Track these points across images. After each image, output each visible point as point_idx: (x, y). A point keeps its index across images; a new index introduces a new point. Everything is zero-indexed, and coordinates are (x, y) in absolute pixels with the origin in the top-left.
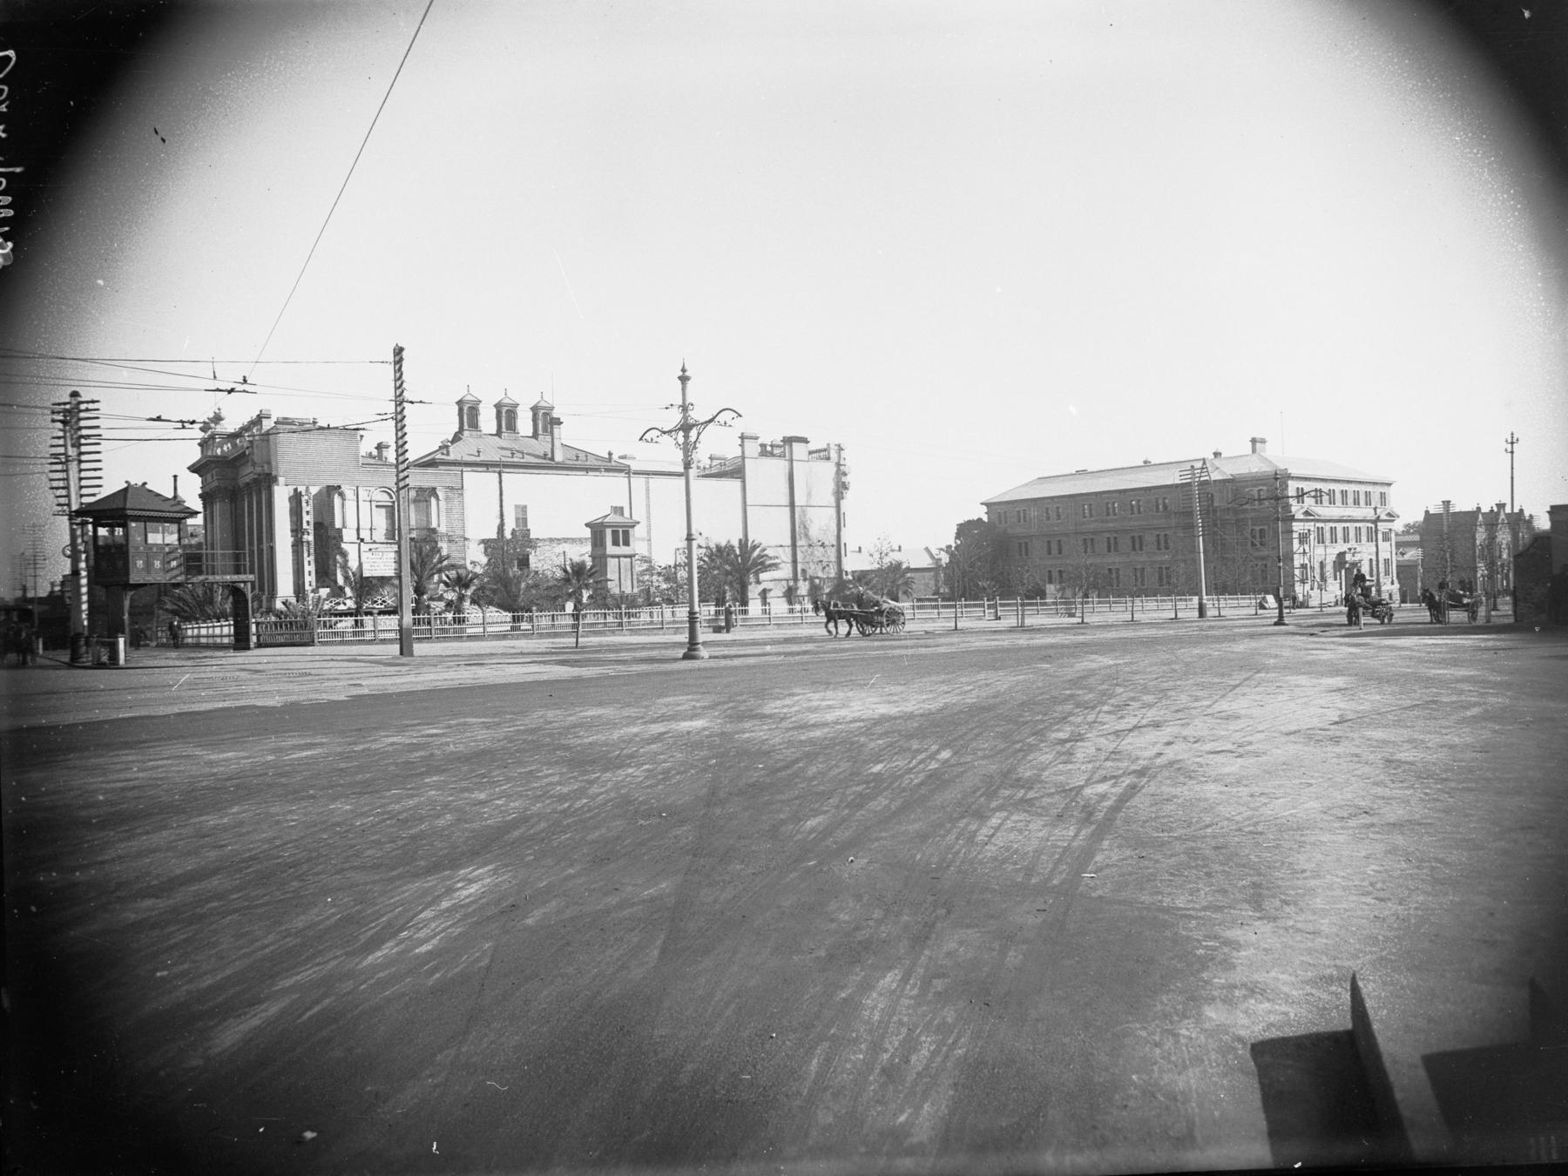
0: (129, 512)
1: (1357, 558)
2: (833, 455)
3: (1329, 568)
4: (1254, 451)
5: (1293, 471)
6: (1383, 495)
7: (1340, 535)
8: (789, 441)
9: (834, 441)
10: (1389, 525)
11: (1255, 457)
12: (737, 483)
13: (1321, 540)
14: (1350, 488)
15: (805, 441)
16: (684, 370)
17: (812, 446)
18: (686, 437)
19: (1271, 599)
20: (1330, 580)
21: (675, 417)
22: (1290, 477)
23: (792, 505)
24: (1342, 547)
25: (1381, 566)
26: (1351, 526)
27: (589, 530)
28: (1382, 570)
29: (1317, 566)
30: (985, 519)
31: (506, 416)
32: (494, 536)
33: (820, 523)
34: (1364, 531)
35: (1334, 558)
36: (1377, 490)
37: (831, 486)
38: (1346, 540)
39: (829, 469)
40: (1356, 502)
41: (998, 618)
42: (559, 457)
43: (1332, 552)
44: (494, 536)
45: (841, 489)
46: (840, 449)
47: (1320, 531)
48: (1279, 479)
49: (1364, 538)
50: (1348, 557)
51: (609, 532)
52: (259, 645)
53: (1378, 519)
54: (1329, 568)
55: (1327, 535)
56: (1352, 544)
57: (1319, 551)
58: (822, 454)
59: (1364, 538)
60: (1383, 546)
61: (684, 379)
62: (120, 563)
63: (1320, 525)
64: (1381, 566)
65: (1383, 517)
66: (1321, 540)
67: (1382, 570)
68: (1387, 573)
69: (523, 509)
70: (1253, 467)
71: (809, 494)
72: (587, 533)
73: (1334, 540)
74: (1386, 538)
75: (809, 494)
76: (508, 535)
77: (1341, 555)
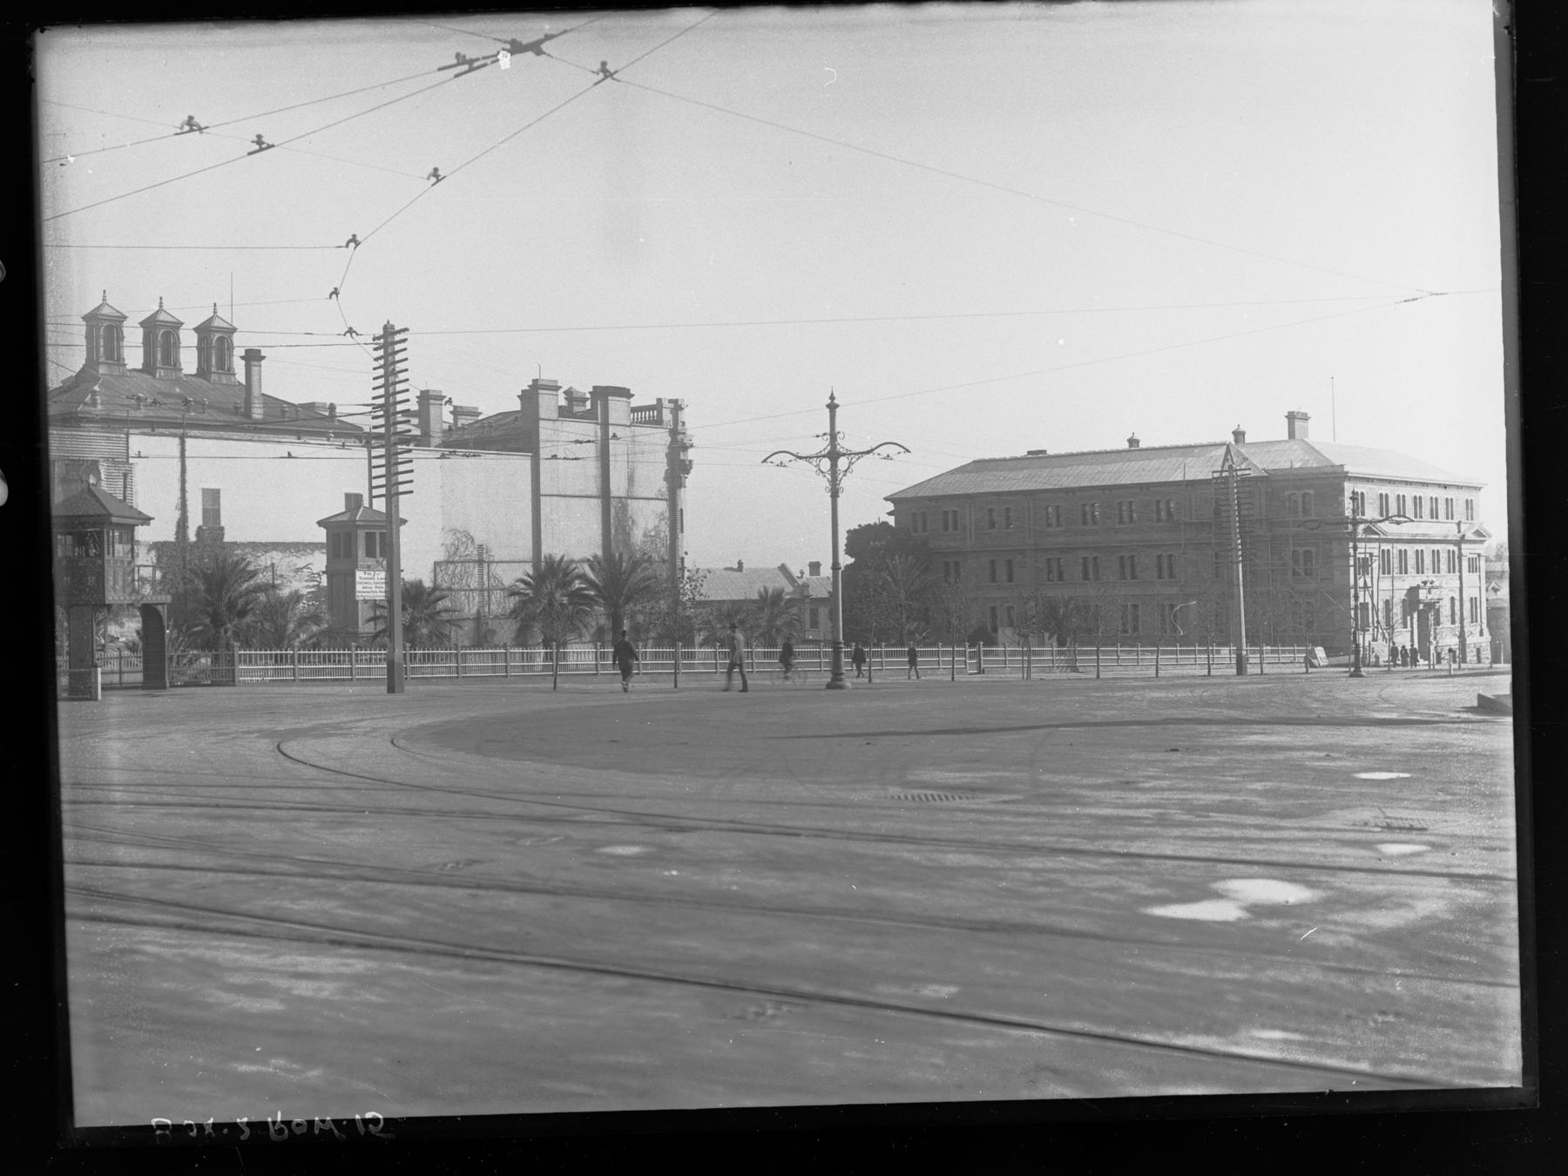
0: (114, 520)
1: (1435, 595)
2: (667, 416)
3: (1397, 610)
4: (1292, 435)
5: (1350, 469)
6: (1469, 504)
7: (1411, 561)
8: (602, 394)
9: (667, 396)
10: (1479, 548)
11: (1295, 446)
12: (522, 463)
13: (1386, 569)
14: (1426, 493)
15: (625, 393)
16: (832, 398)
17: (635, 402)
18: (834, 466)
19: (1320, 652)
20: (1399, 628)
21: (823, 445)
22: (1346, 477)
23: (605, 494)
24: (1416, 580)
25: (1467, 605)
26: (1427, 549)
27: (323, 531)
28: (1467, 614)
29: (1381, 606)
30: (891, 521)
31: (160, 334)
32: (172, 538)
33: (647, 518)
34: (1444, 556)
35: (1400, 595)
36: (1459, 498)
37: (662, 467)
38: (1420, 569)
39: (658, 439)
40: (1434, 514)
41: (981, 671)
42: (258, 413)
43: (1404, 584)
44: (172, 538)
45: (678, 469)
46: (677, 407)
47: (1385, 555)
48: (1329, 482)
49: (1444, 567)
50: (1422, 594)
51: (361, 534)
52: (172, 686)
53: (1463, 540)
54: (1397, 610)
55: (1395, 562)
56: (1428, 575)
57: (1385, 584)
58: (651, 415)
59: (1444, 567)
60: (1470, 579)
61: (832, 407)
62: (91, 580)
63: (1385, 547)
64: (1467, 605)
65: (1470, 536)
66: (1386, 569)
67: (1467, 614)
68: (1474, 619)
69: (212, 497)
70: (1292, 459)
71: (631, 480)
72: (321, 535)
73: (1404, 570)
74: (1473, 568)
75: (631, 480)
76: (192, 537)
77: (1413, 591)
